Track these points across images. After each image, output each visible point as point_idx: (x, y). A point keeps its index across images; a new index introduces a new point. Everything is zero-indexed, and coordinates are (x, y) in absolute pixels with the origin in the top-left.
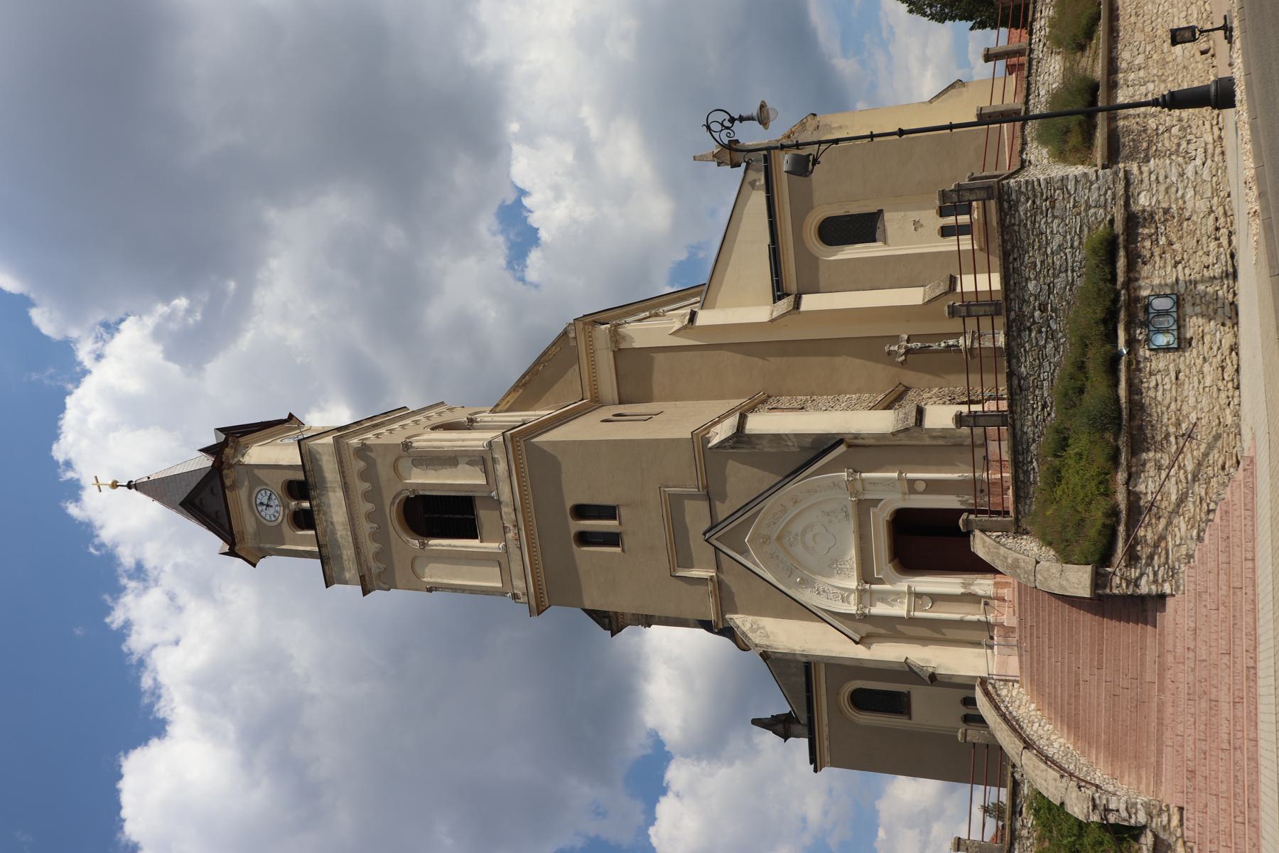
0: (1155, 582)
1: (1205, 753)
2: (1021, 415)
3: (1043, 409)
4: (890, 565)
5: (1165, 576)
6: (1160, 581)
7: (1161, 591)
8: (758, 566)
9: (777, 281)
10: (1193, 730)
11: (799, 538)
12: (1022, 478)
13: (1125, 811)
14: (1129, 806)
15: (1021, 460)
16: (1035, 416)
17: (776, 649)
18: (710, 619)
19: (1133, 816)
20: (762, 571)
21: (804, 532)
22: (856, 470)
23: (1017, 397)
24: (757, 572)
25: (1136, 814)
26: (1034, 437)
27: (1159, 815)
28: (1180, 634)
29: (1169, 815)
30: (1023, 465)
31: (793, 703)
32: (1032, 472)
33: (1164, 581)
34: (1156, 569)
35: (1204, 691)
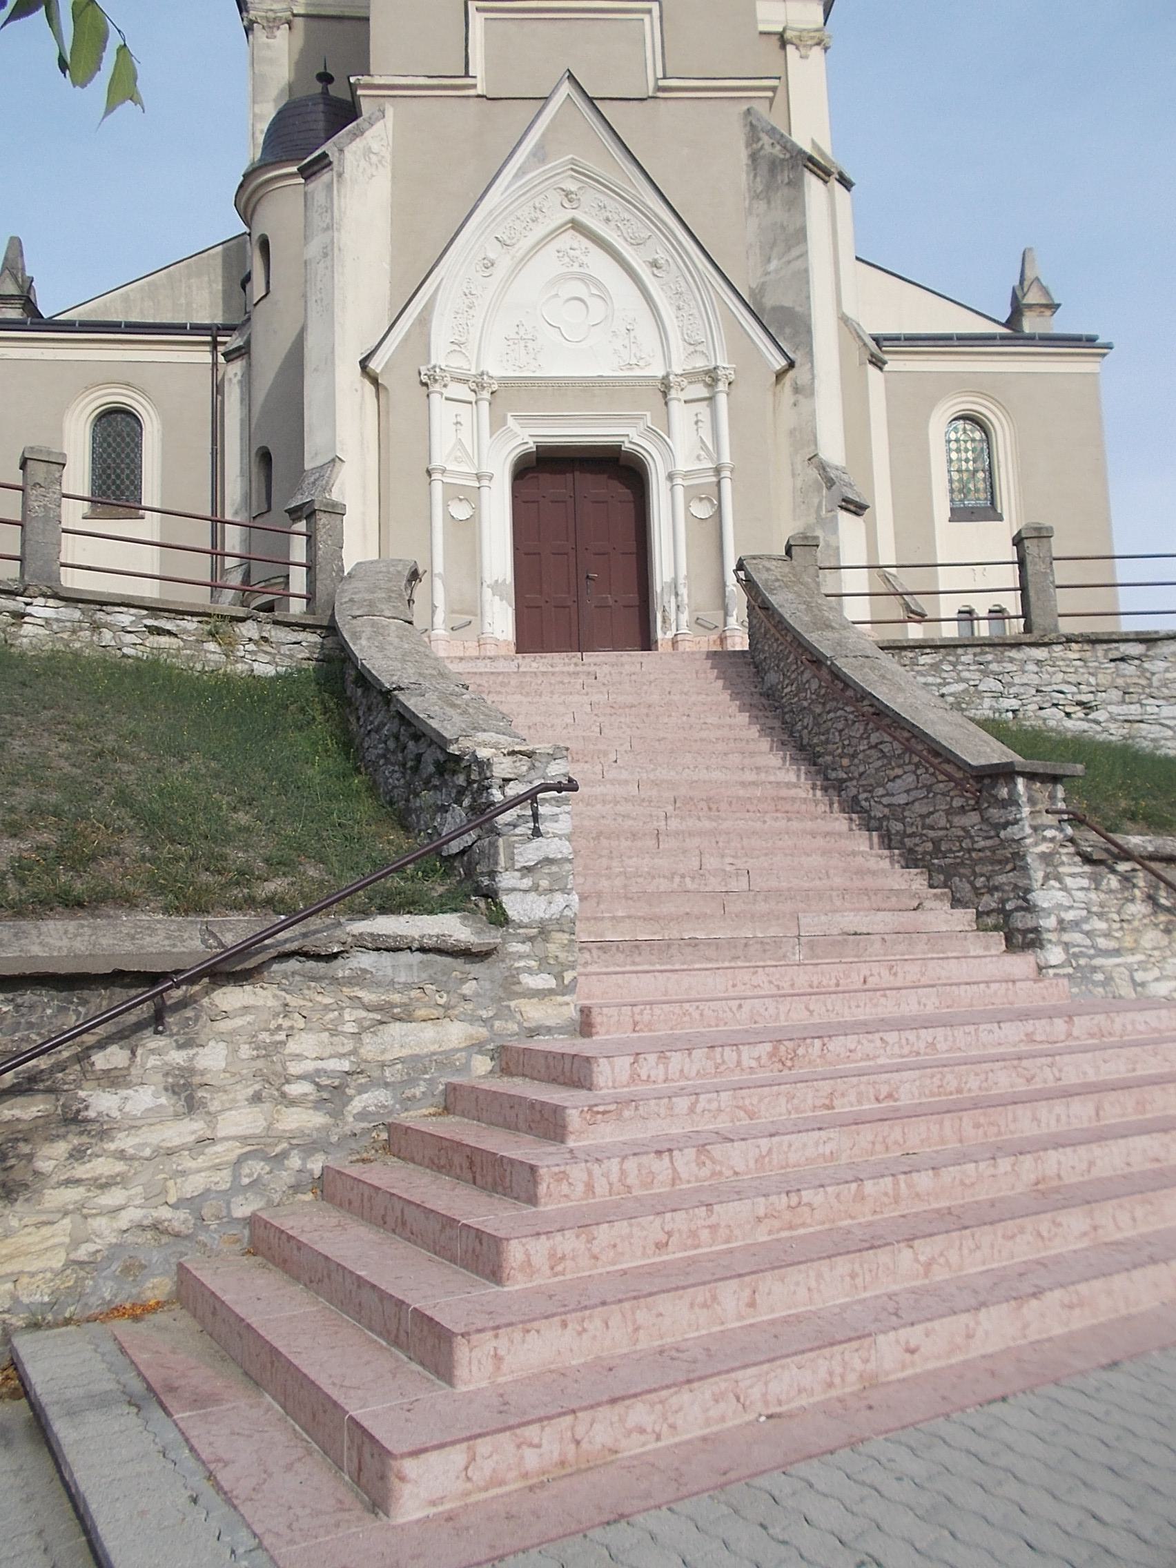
0: (1062, 926)
1: (890, 1096)
2: (1063, 660)
3: (1079, 703)
4: (531, 444)
5: (1076, 950)
6: (1066, 937)
7: (1050, 941)
8: (517, 176)
9: (906, 339)
10: (896, 1050)
11: (576, 268)
12: (923, 660)
13: (541, 856)
14: (554, 869)
15: (963, 659)
16: (1065, 688)
17: (338, 191)
18: (372, 70)
19: (527, 883)
20: (506, 183)
21: (587, 279)
22: (733, 386)
23: (1100, 653)
24: (505, 172)
25: (535, 888)
26: (1014, 685)
27: (544, 964)
28: (995, 993)
29: (551, 992)
30: (951, 663)
31: (149, 283)
32: (939, 680)
33: (1067, 946)
34: (1086, 927)
35: (1033, 1077)
